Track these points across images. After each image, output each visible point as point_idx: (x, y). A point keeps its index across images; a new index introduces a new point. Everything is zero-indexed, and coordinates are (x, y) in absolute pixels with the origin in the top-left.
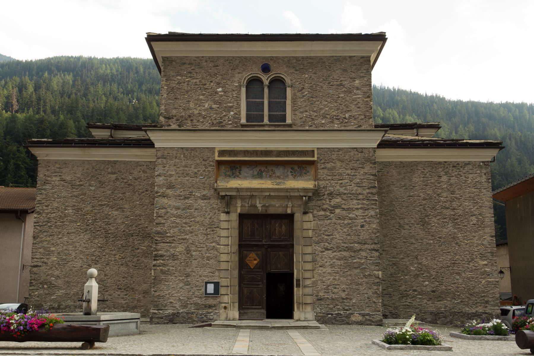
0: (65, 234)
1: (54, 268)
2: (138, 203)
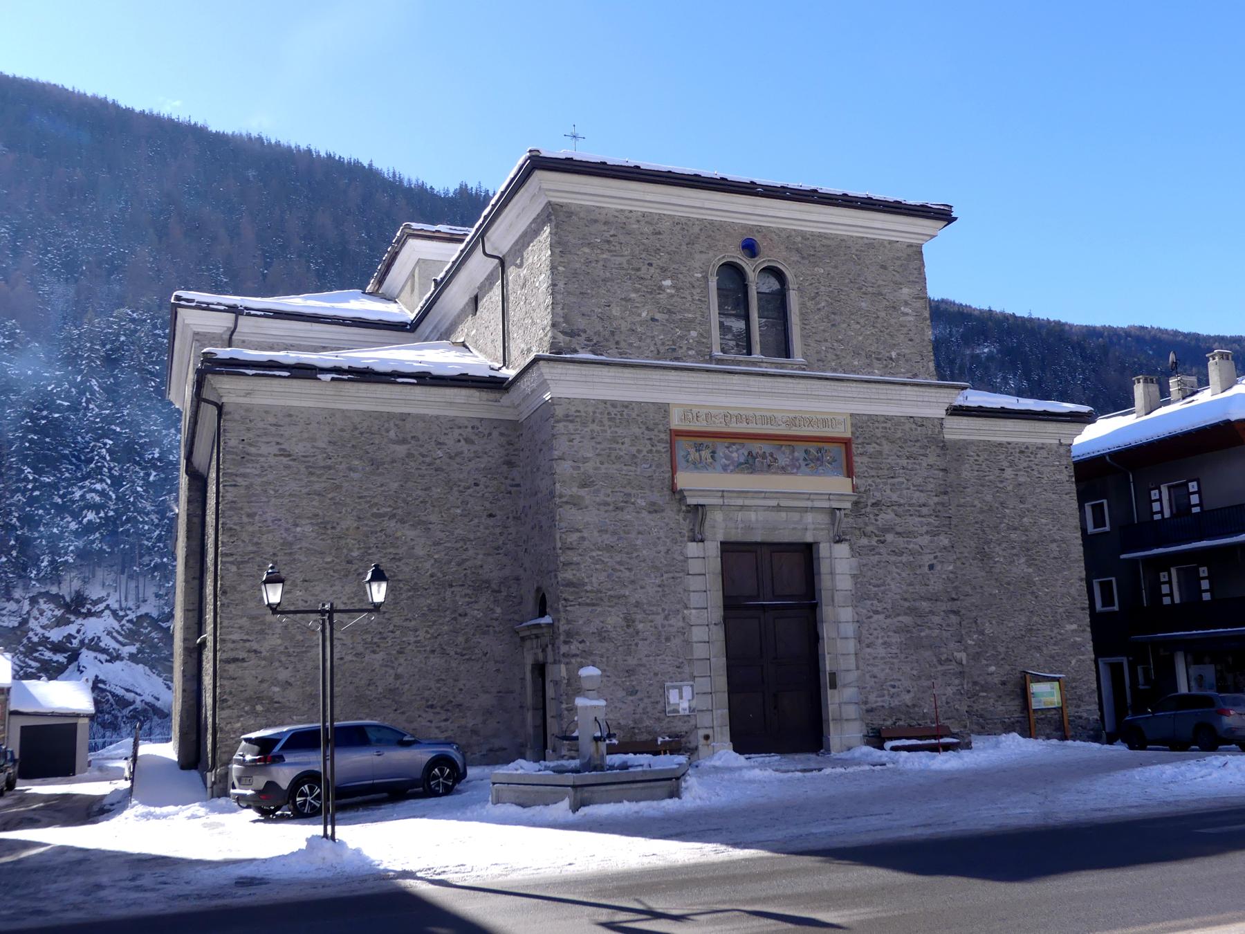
0: (298, 582)
1: (277, 664)
2: (459, 511)
